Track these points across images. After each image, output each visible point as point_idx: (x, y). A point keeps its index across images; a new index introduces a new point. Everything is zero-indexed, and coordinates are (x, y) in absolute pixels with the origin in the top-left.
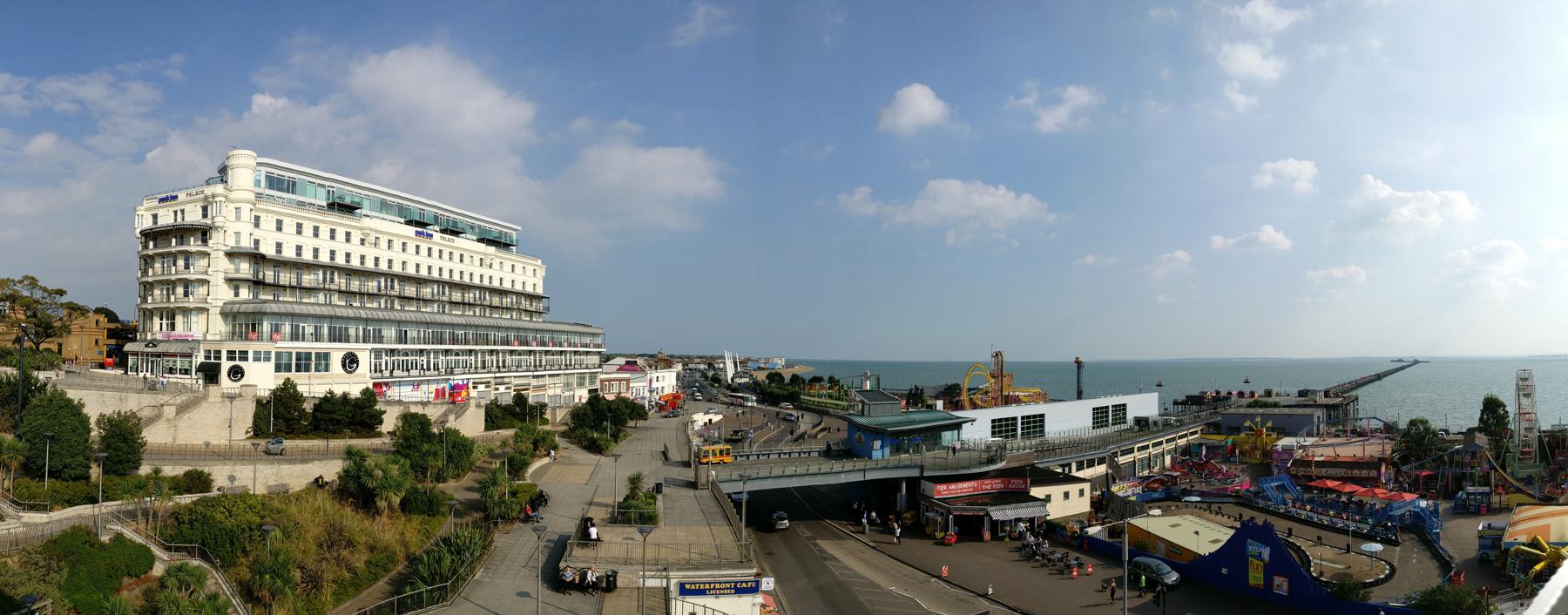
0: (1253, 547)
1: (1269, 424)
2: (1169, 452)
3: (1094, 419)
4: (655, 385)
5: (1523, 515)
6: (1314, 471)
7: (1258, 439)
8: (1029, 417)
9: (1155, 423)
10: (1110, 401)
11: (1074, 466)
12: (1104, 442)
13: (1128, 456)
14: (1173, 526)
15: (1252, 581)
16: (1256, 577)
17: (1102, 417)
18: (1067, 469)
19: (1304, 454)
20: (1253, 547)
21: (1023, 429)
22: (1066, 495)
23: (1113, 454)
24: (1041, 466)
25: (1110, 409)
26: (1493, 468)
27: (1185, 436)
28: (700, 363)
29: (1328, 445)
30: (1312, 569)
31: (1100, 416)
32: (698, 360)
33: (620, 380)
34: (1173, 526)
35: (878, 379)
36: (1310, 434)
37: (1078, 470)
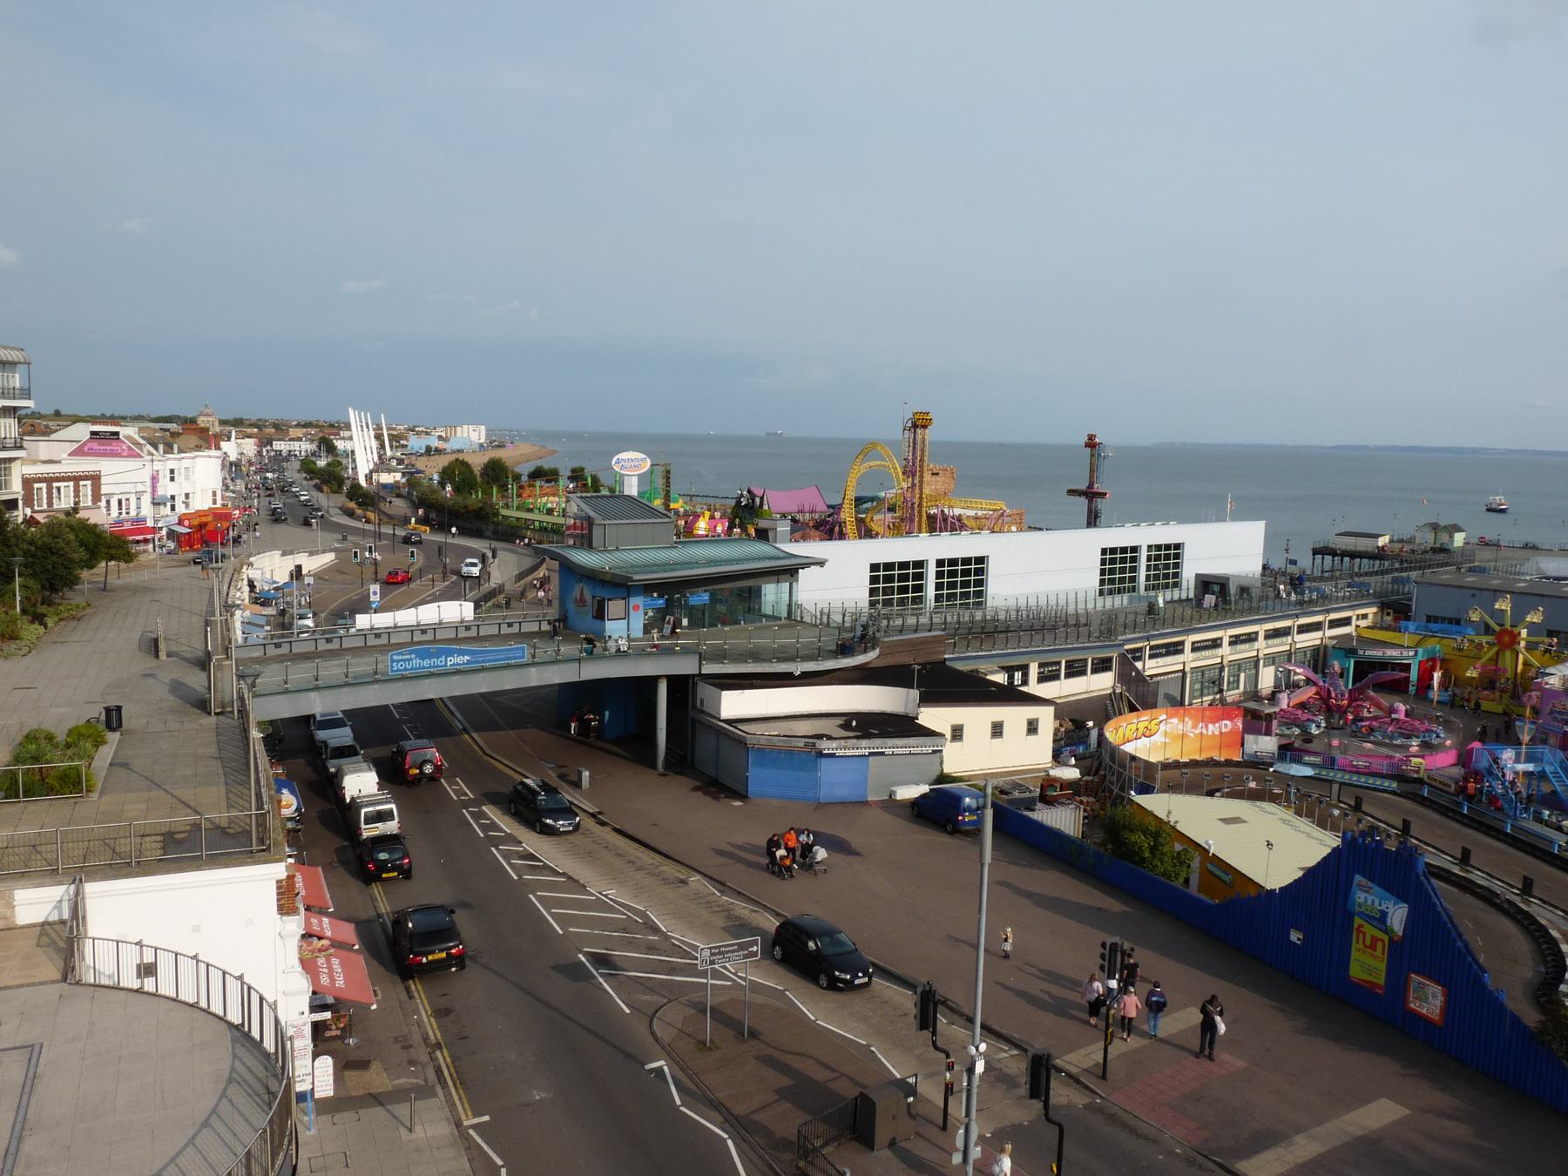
0: (1366, 896)
1: (1535, 617)
2: (1272, 659)
3: (1103, 572)
4: (166, 488)
9: (1244, 590)
10: (1143, 536)
11: (1034, 670)
12: (1109, 626)
13: (1170, 659)
14: (1226, 821)
15: (1356, 972)
17: (1123, 570)
18: (1018, 676)
20: (1366, 896)
22: (997, 730)
23: (1134, 651)
24: (961, 666)
25: (1144, 554)
27: (1317, 627)
28: (300, 439)
31: (1117, 563)
32: (299, 432)
33: (76, 479)
34: (1226, 821)
35: (668, 472)
37: (1042, 679)
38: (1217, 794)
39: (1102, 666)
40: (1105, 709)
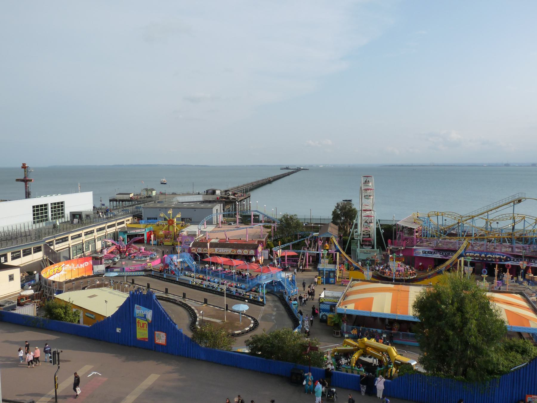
1: (179, 216)
2: (100, 238)
3: (34, 215)
5: (355, 289)
6: (209, 250)
7: (171, 227)
8: (37, 206)
9: (87, 216)
10: (49, 200)
11: (9, 256)
12: (39, 234)
14: (90, 297)
15: (139, 336)
16: (142, 333)
19: (204, 238)
21: (52, 212)
26: (338, 251)
27: (113, 225)
29: (221, 231)
30: (197, 323)
34: (90, 297)
36: (210, 223)
37: (13, 258)
38: (86, 288)
39: (38, 250)
40: (40, 266)
